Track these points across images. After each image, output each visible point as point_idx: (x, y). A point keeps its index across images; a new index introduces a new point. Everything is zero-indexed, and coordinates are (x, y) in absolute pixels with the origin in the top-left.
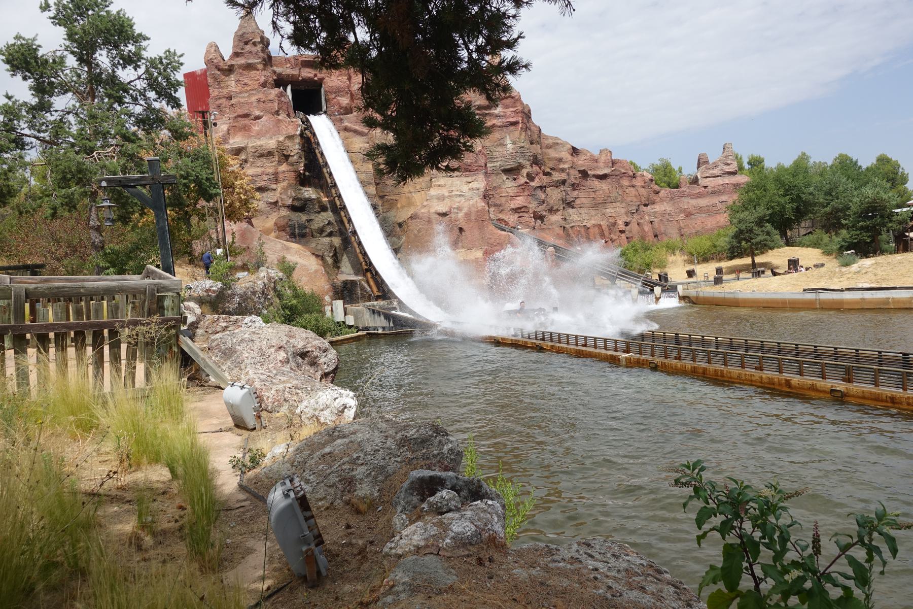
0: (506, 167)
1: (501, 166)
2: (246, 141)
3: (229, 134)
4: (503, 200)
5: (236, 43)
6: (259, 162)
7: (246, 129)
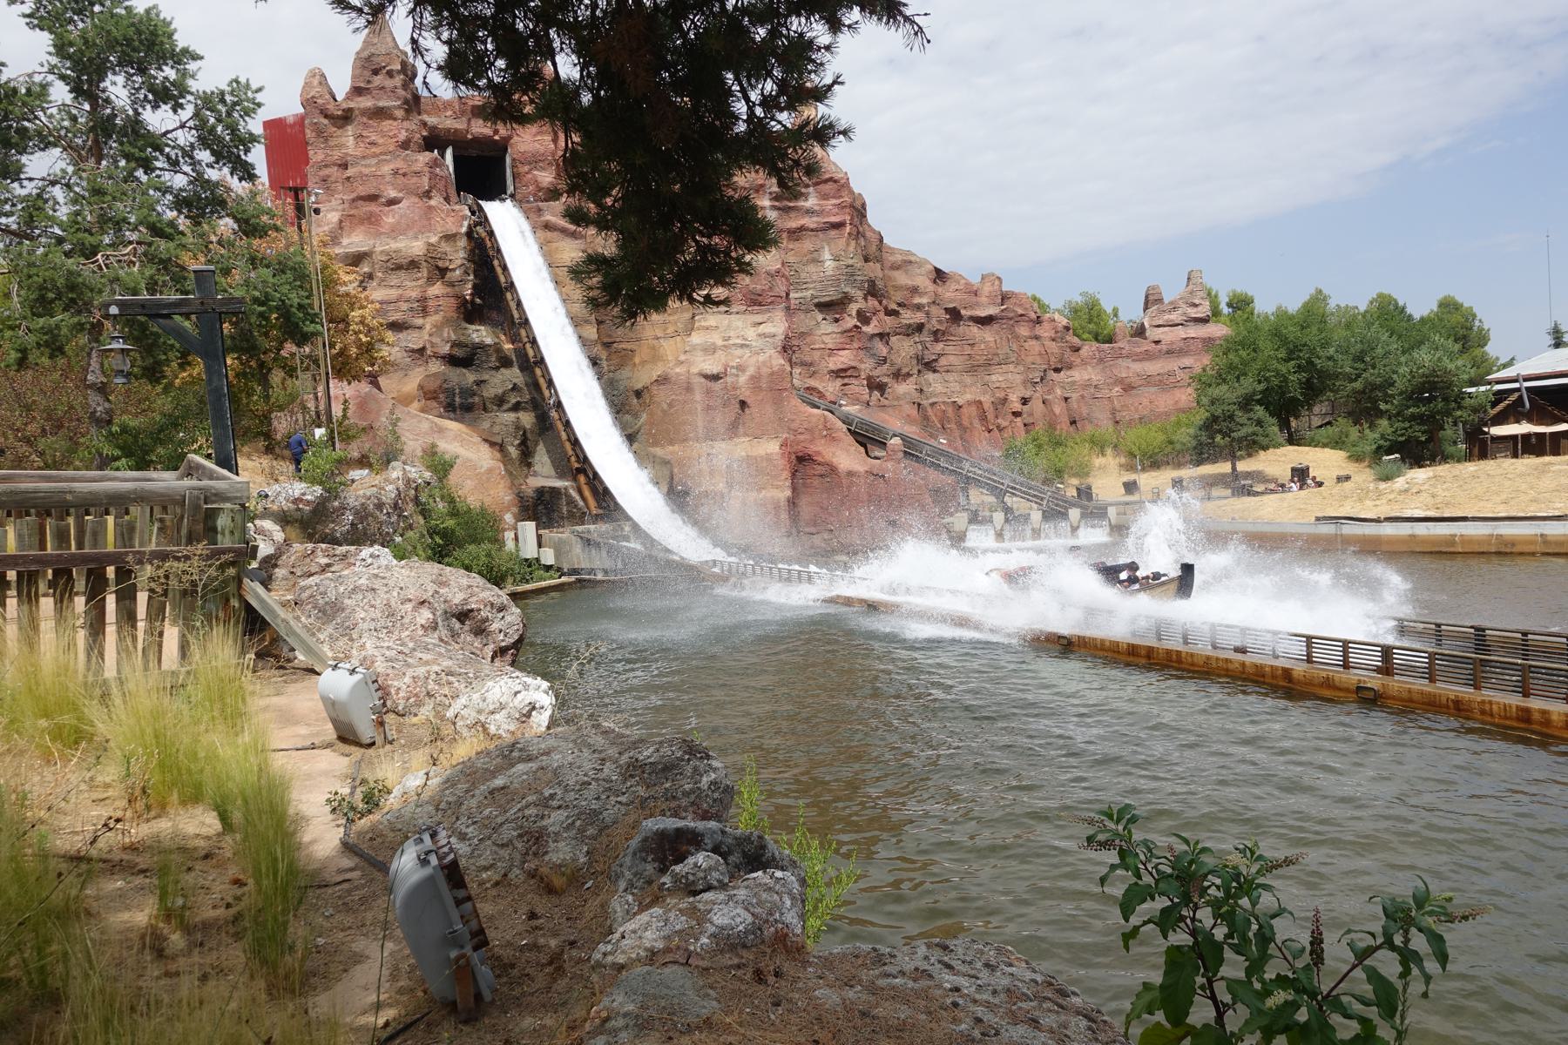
0: (822, 300)
2: (371, 242)
5: (358, 71)
6: (394, 279)
7: (371, 220)
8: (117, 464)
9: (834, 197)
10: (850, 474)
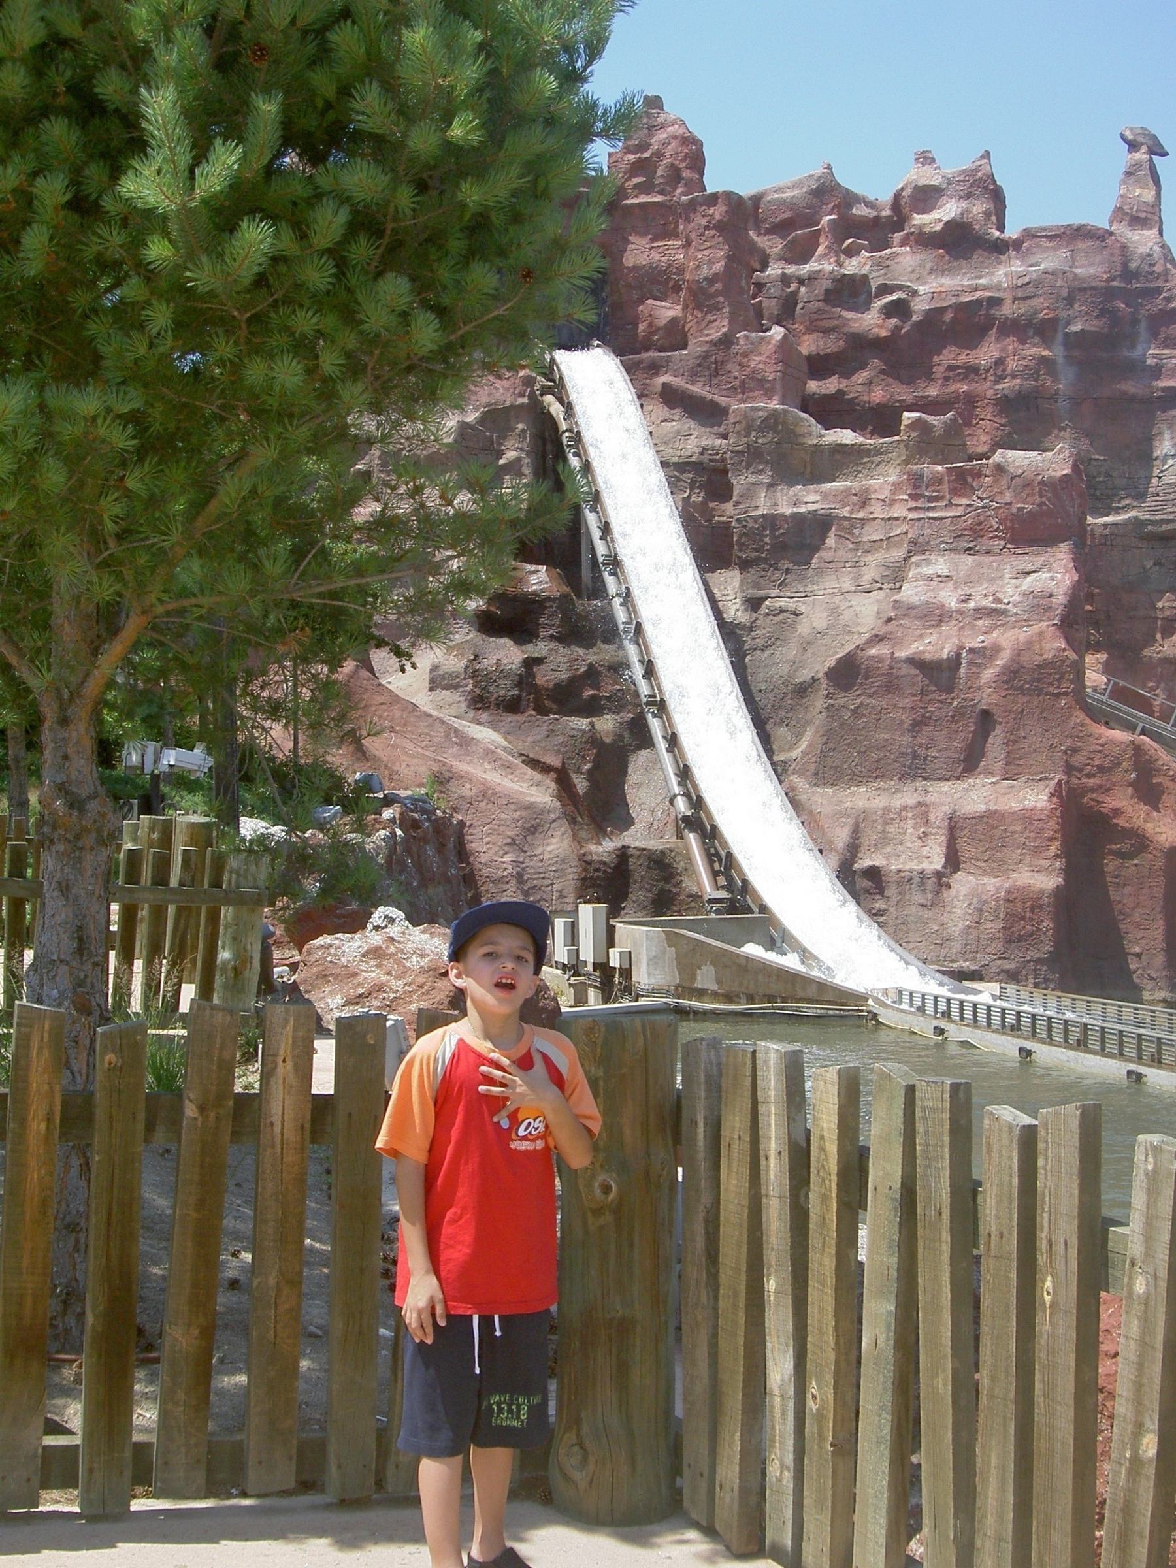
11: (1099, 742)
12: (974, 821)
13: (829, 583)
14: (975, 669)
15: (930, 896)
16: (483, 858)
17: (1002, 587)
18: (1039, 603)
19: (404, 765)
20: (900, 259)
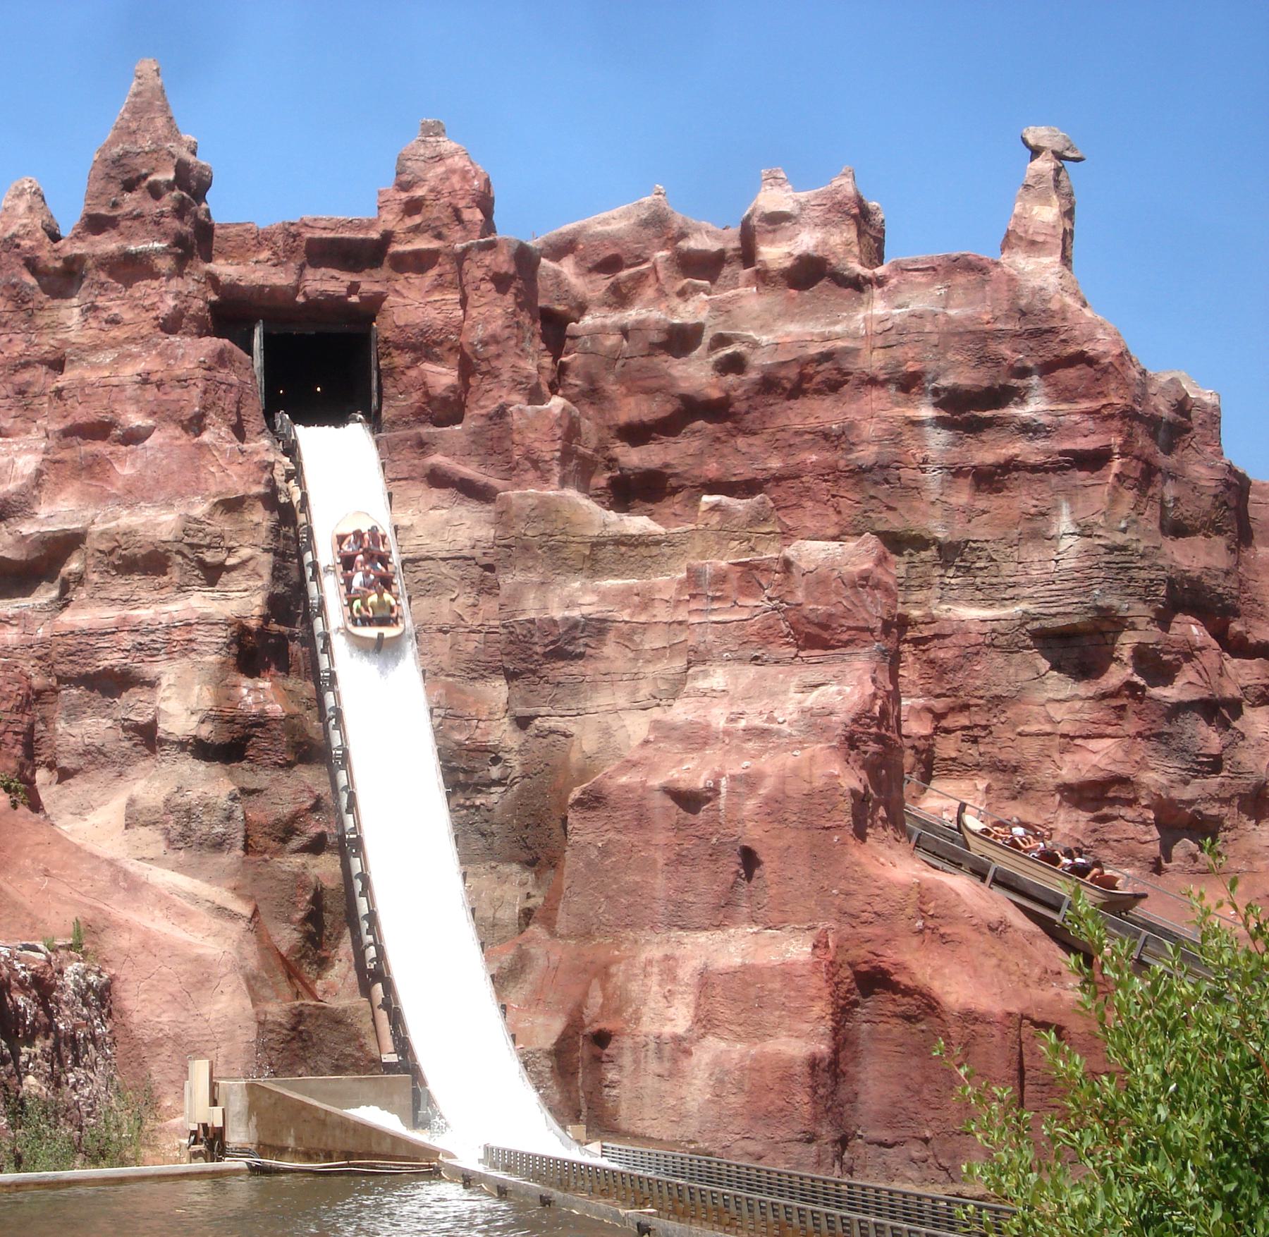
0: (1048, 624)
1: (1027, 617)
2: (89, 513)
3: (38, 485)
4: (1030, 749)
5: (99, 185)
6: (120, 587)
7: (93, 469)
8: (223, 1037)
9: (1086, 396)
10: (969, 1017)
11: (879, 884)
12: (726, 977)
13: (603, 699)
14: (735, 800)
15: (667, 1065)
16: (136, 1018)
17: (784, 703)
18: (815, 721)
19: (53, 913)
20: (744, 302)
